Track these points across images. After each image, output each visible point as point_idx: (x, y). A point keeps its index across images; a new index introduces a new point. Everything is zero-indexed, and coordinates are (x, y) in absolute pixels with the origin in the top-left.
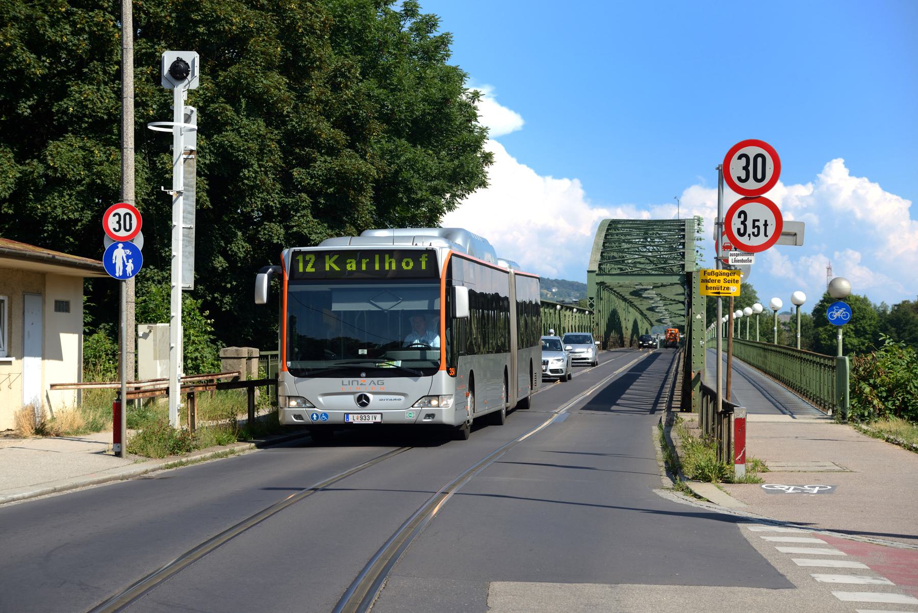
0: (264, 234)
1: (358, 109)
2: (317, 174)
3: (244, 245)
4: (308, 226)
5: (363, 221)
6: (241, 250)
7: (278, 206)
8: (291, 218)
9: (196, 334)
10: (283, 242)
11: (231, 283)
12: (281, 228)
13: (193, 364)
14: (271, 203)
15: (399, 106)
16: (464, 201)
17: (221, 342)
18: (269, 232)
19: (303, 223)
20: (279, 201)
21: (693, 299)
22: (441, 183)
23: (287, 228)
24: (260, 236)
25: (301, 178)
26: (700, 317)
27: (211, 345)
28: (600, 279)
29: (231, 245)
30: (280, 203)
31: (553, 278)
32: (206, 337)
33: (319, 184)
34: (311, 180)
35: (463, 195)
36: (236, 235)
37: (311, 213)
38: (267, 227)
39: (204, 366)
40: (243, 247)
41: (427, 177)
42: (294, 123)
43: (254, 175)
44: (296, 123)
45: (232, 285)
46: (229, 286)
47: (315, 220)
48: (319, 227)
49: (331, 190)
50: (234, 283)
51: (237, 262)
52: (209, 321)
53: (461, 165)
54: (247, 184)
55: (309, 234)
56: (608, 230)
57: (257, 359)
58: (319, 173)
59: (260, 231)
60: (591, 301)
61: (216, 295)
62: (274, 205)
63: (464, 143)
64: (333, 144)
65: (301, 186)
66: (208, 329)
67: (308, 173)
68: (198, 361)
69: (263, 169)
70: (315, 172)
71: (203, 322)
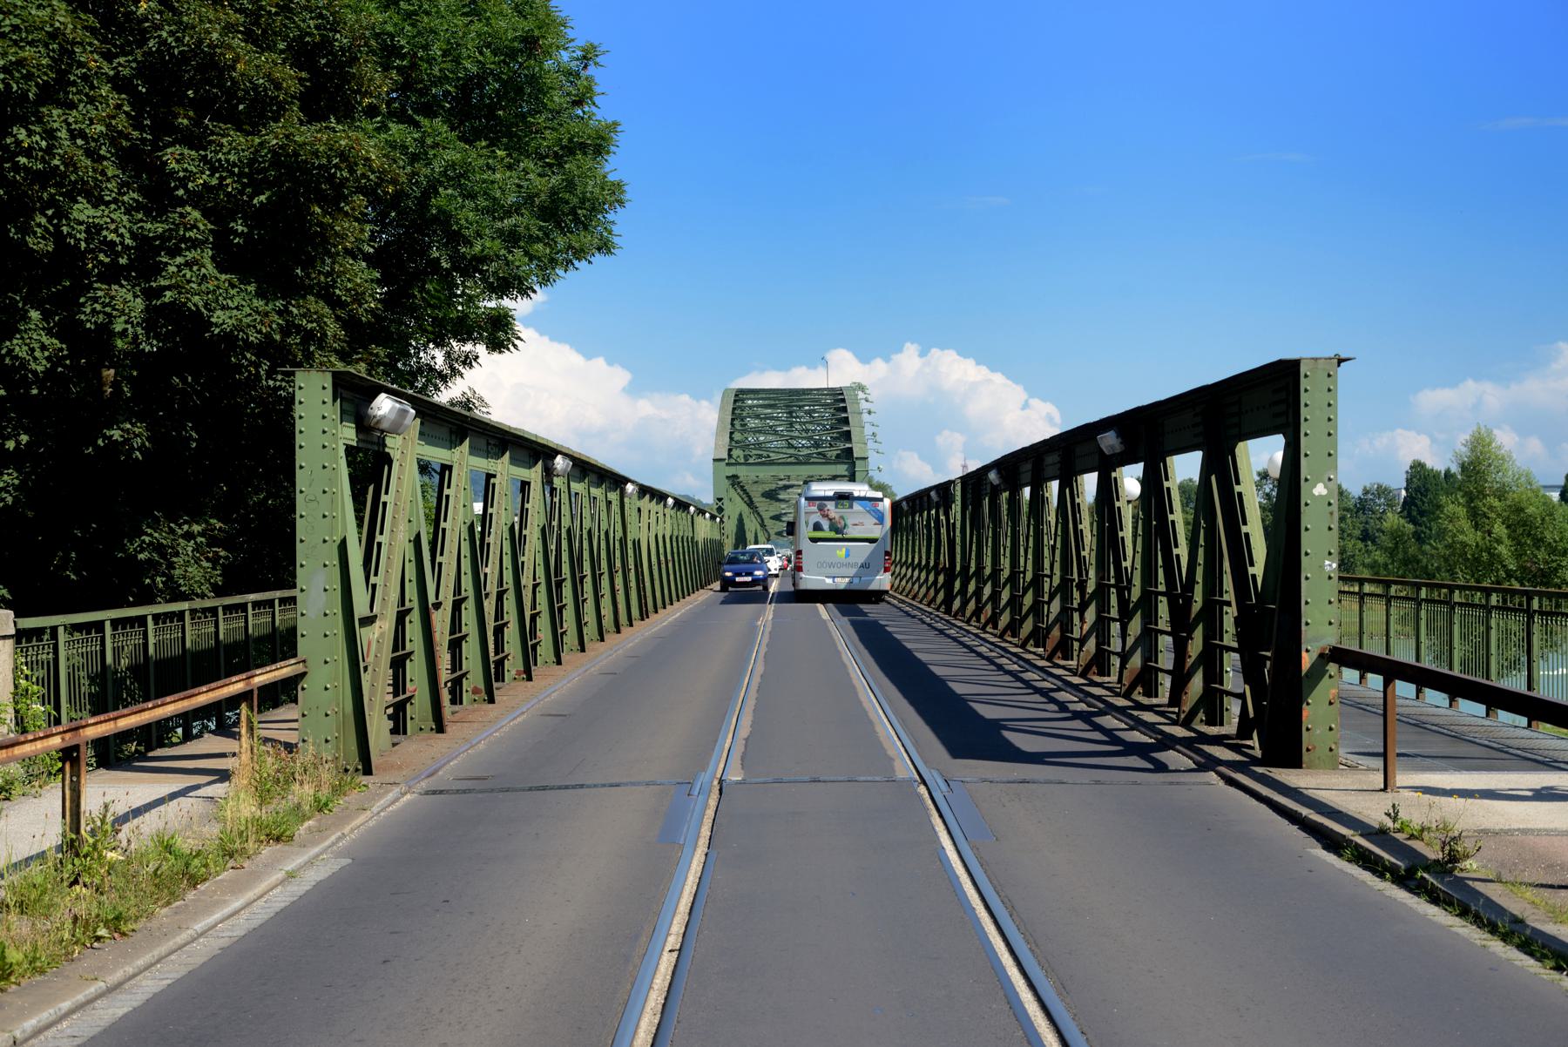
0: (94, 311)
1: (331, 30)
2: (227, 161)
3: (45, 339)
4: (203, 288)
5: (348, 290)
6: (38, 354)
7: (128, 241)
8: (163, 270)
10: (139, 330)
12: (136, 296)
14: (112, 237)
15: (426, 47)
16: (571, 273)
18: (104, 305)
19: (189, 282)
20: (130, 231)
21: (1303, 439)
22: (525, 221)
23: (151, 294)
24: (83, 317)
25: (185, 170)
26: (1324, 492)
28: (731, 471)
30: (133, 236)
33: (231, 185)
34: (212, 175)
35: (570, 262)
36: (25, 318)
37: (213, 258)
38: (100, 293)
40: (43, 348)
41: (496, 210)
42: (164, 34)
43: (44, 144)
44: (171, 33)
45: (18, 443)
47: (223, 277)
48: (233, 292)
49: (263, 198)
50: (24, 438)
53: (570, 185)
54: (25, 168)
55: (210, 310)
56: (735, 401)
58: (232, 158)
59: (83, 305)
60: (720, 504)
62: (118, 240)
63: (570, 140)
64: (265, 89)
65: (187, 190)
67: (204, 159)
69: (80, 142)
70: (220, 155)
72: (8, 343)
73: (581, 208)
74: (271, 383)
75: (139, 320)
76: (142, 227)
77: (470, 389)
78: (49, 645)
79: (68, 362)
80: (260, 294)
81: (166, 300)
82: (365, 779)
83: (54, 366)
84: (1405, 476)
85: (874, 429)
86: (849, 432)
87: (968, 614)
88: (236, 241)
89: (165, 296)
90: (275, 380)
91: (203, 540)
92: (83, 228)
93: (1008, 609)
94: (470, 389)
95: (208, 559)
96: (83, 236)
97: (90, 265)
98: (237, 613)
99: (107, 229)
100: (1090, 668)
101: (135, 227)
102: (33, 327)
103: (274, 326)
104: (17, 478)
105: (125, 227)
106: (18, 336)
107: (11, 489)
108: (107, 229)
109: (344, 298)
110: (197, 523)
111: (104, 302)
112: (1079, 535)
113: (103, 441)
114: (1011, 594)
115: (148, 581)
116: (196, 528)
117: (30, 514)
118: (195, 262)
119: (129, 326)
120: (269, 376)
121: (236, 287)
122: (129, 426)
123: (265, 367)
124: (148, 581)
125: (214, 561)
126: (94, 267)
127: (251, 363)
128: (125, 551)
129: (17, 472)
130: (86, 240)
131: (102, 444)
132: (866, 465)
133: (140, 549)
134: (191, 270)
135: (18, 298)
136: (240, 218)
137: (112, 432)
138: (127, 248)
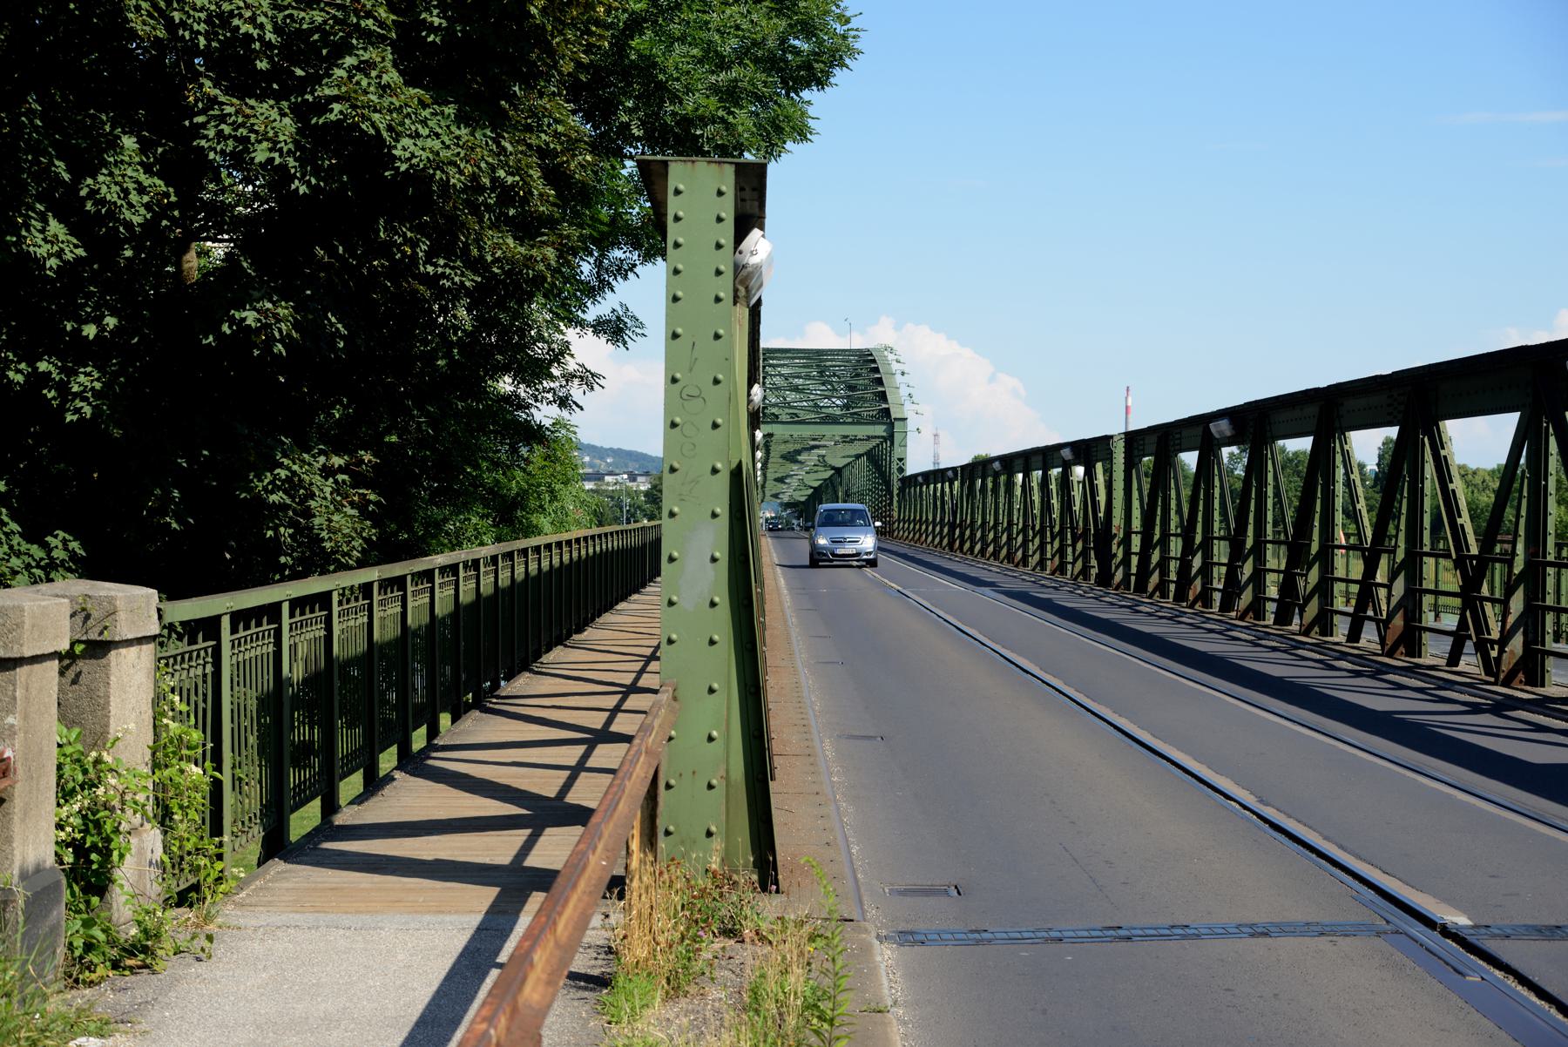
3: (142, 177)
6: (134, 197)
10: (291, 162)
11: (98, 321)
12: (283, 115)
14: (246, 28)
17: (61, 534)
20: (273, 19)
23: (301, 113)
24: (203, 143)
27: (24, 546)
29: (94, 178)
30: (277, 30)
31: (607, 446)
36: (114, 144)
38: (228, 110)
40: (141, 190)
45: (102, 328)
46: (90, 331)
50: (111, 322)
51: (119, 245)
57: (148, 650)
59: (204, 125)
61: (43, 366)
62: (255, 33)
72: (89, 181)
73: (817, 62)
74: (430, 269)
75: (291, 146)
76: (291, 16)
77: (621, 305)
78: (205, 649)
79: (176, 213)
80: (461, 119)
81: (332, 117)
82: (769, 906)
83: (157, 218)
84: (1377, 452)
85: (910, 390)
86: (884, 393)
87: (1150, 588)
88: (430, 39)
89: (332, 110)
90: (436, 265)
91: (345, 477)
92: (203, 15)
93: (1251, 586)
94: (621, 305)
95: (352, 504)
96: (202, 27)
97: (191, 99)
98: (422, 584)
99: (241, 16)
100: (1516, 676)
101: (280, 16)
103: (483, 165)
104: (98, 380)
105: (266, 16)
106: (104, 171)
107: (89, 395)
108: (241, 16)
109: (552, 146)
110: (339, 456)
111: (234, 122)
112: (1032, 502)
113: (230, 327)
114: (1255, 568)
115: (270, 533)
116: (337, 461)
117: (117, 433)
118: (369, 65)
119: (276, 155)
120: (428, 261)
121: (428, 106)
122: (269, 305)
123: (424, 247)
124: (270, 533)
125: (362, 506)
126: (197, 100)
127: (407, 241)
128: (250, 490)
129: (99, 370)
130: (207, 35)
131: (228, 332)
132: (905, 426)
133: (268, 488)
134: (367, 76)
135: (105, 118)
136: (435, 7)
137: (244, 314)
138: (269, 45)
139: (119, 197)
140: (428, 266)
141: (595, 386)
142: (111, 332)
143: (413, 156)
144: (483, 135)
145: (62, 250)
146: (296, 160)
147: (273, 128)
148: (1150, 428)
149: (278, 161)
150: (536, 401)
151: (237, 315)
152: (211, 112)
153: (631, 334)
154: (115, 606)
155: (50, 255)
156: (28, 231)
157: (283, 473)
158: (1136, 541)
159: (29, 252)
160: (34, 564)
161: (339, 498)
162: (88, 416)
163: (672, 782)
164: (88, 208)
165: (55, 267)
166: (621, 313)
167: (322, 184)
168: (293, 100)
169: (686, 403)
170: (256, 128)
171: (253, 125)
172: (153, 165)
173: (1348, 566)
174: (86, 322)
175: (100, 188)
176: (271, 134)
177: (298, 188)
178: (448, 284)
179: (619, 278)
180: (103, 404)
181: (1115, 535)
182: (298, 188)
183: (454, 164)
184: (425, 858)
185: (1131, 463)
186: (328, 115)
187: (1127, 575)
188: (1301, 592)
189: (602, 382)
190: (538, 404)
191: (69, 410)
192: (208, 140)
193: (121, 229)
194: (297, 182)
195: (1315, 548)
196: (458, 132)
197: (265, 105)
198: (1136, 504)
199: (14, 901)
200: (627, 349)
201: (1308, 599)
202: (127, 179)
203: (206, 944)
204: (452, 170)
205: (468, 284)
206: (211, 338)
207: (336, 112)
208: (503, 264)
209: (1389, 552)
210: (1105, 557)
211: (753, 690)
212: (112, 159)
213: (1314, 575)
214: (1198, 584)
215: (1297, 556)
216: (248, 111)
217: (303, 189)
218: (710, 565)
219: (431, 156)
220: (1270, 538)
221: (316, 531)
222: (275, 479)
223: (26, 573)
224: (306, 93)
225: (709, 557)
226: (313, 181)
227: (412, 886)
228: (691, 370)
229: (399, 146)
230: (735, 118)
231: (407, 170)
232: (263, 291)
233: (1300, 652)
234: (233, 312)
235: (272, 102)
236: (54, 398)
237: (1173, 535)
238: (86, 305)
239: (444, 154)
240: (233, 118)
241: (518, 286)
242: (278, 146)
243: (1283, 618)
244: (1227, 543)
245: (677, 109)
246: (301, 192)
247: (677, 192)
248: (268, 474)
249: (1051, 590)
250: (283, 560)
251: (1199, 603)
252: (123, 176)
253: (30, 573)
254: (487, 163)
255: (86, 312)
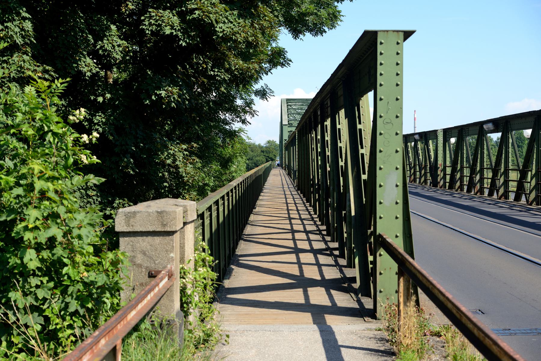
0: (150, 24)
9: (49, 173)
10: (180, 34)
11: (103, 96)
12: (174, 16)
13: (42, 260)
23: (182, 15)
24: (144, 27)
29: (102, 41)
32: (78, 179)
36: (109, 29)
38: (153, 14)
39: (74, 264)
46: (100, 99)
50: (108, 96)
52: (85, 138)
59: (144, 20)
66: (84, 158)
68: (59, 251)
71: (70, 139)
72: (100, 42)
74: (212, 73)
75: (179, 28)
77: (265, 84)
80: (240, 16)
81: (195, 16)
90: (214, 71)
91: (187, 153)
93: (503, 187)
94: (265, 84)
97: (124, 10)
102: (113, 34)
103: (249, 33)
104: (104, 118)
106: (106, 39)
113: (155, 97)
115: (160, 174)
116: (184, 147)
120: (212, 70)
123: (210, 65)
126: (126, 10)
139: (112, 48)
140: (211, 72)
141: (255, 115)
142: (108, 100)
143: (224, 30)
144: (248, 22)
145: (92, 69)
146: (181, 33)
147: (171, 21)
148: (455, 127)
149: (174, 33)
150: (233, 121)
151: (158, 93)
152: (146, 15)
153: (269, 96)
154: (187, 209)
155: (88, 71)
156: (80, 62)
157: (172, 152)
158: (449, 170)
159: (81, 70)
160: (81, 188)
161: (185, 161)
162: (101, 132)
163: (382, 272)
164: (100, 53)
165: (89, 76)
166: (265, 88)
167: (191, 42)
168: (177, 10)
169: (385, 125)
170: (165, 21)
171: (163, 20)
172: (121, 36)
173: (514, 176)
174: (99, 96)
175: (104, 45)
176: (170, 23)
177: (182, 44)
178: (219, 79)
179: (264, 74)
180: (106, 127)
181: (439, 167)
182: (182, 44)
183: (238, 33)
184: (271, 301)
185: (446, 140)
186: (193, 15)
187: (445, 183)
188: (498, 186)
189: (257, 113)
190: (234, 123)
191: (93, 129)
192: (146, 26)
193: (112, 60)
194: (181, 41)
195: (478, 169)
196: (239, 21)
197: (167, 12)
198: (448, 155)
199: (176, 324)
200: (268, 101)
201: (500, 188)
202: (114, 41)
203: (227, 339)
204: (238, 36)
205: (226, 78)
206: (148, 102)
207: (197, 14)
208: (238, 71)
209: (530, 171)
210: (434, 175)
211: (408, 236)
212: (108, 34)
213: (478, 177)
214: (458, 184)
215: (473, 171)
216: (160, 15)
217: (184, 44)
218: (395, 188)
219: (231, 30)
220: (465, 166)
221: (180, 174)
222: (168, 154)
223: (78, 192)
224: (182, 7)
225: (395, 185)
226: (188, 41)
227: (276, 313)
228: (387, 112)
229: (218, 27)
230: (320, 12)
231: (222, 36)
232: (167, 83)
233: (531, 212)
234: (156, 91)
235: (169, 11)
236: (87, 125)
237: (465, 167)
238: (98, 89)
239: (235, 29)
240: (155, 17)
241: (244, 79)
242: (174, 28)
243: (491, 194)
244: (491, 170)
245: (299, 10)
246: (183, 45)
247: (381, 43)
248: (166, 153)
249: (414, 189)
250: (165, 184)
251: (479, 193)
252: (112, 40)
253: (80, 191)
254: (250, 32)
255: (99, 92)
